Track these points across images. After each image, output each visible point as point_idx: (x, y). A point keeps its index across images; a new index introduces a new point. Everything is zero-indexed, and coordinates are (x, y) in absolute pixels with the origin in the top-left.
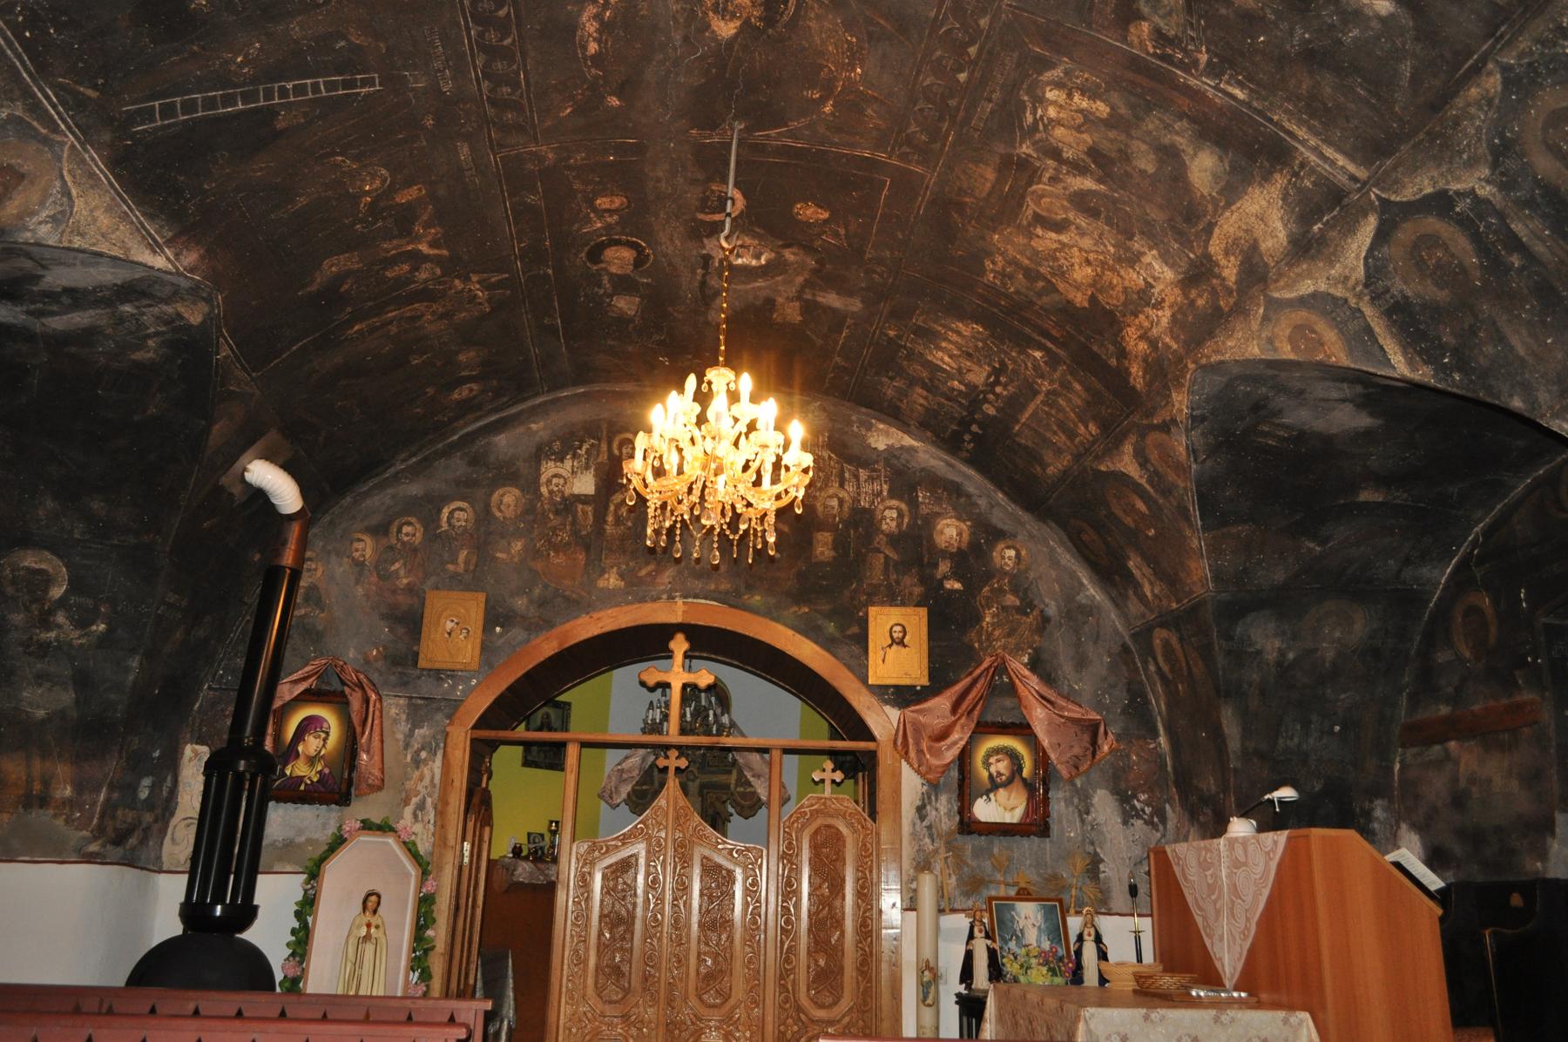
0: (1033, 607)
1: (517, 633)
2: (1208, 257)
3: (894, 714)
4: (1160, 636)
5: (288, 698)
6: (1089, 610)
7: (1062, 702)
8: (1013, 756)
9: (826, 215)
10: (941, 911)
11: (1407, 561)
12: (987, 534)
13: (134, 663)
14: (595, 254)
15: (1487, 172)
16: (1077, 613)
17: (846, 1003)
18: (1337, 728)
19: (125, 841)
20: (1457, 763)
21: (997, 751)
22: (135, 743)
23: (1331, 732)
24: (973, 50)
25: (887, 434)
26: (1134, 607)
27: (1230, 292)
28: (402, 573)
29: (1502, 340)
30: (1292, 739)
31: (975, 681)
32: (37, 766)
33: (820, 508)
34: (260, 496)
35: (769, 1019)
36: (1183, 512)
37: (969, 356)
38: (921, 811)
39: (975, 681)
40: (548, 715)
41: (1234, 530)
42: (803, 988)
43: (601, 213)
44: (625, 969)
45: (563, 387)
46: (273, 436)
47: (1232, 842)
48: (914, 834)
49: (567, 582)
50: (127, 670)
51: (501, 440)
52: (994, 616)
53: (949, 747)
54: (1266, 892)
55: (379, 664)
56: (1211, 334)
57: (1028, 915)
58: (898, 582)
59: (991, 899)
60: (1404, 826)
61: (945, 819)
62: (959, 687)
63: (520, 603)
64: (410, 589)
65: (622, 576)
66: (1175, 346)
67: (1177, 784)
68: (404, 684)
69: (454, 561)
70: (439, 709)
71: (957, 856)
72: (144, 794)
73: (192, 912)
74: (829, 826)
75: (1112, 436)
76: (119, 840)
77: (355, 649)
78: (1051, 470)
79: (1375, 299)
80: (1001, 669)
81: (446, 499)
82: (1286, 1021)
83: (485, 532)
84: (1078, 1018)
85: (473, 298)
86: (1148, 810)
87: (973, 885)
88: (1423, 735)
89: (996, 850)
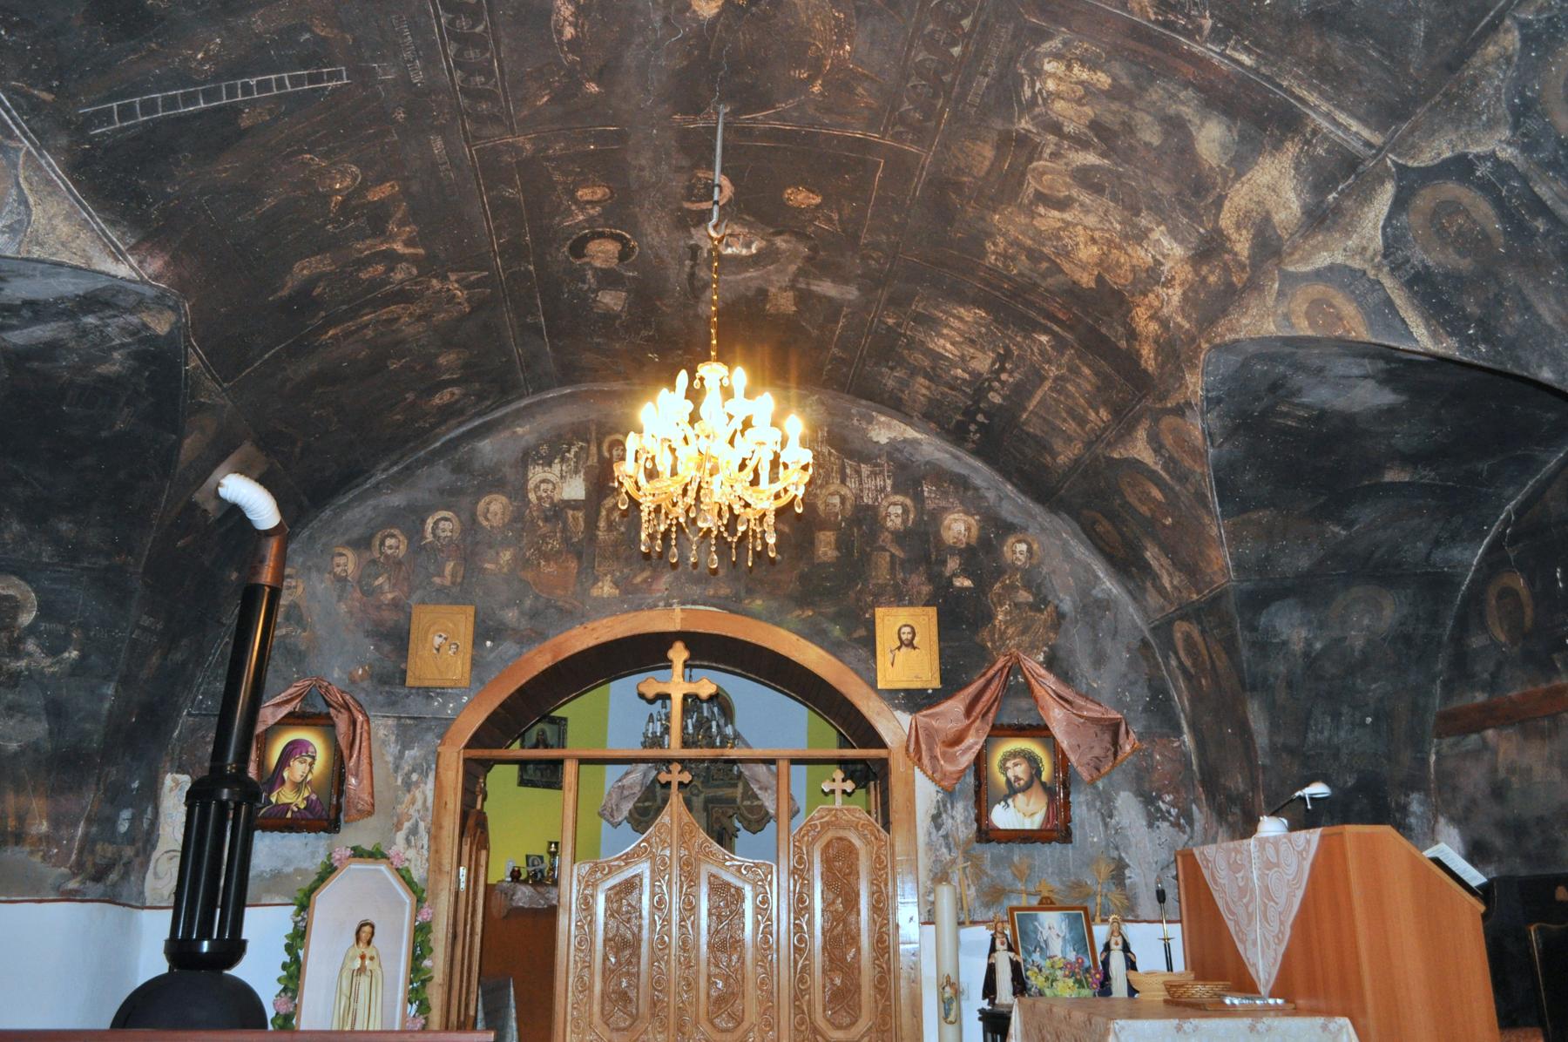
0: (1047, 603)
1: (509, 647)
3: (905, 719)
4: (1180, 629)
5: (271, 722)
6: (1105, 605)
7: (1080, 702)
8: (1031, 760)
9: (818, 200)
10: (961, 924)
11: (1437, 543)
12: (997, 528)
13: (110, 690)
14: (578, 248)
15: (1508, 133)
16: (1094, 608)
18: (1369, 720)
19: (105, 876)
21: (1014, 754)
22: (113, 773)
24: (966, 23)
25: (889, 427)
26: (1153, 600)
27: (1243, 267)
28: (386, 587)
29: (1528, 308)
30: (1322, 732)
33: (821, 507)
34: (235, 512)
37: (972, 341)
38: (936, 819)
39: (989, 682)
40: (543, 732)
41: (1254, 516)
42: (819, 1008)
43: (582, 205)
44: (632, 994)
45: (549, 388)
46: (247, 448)
47: (1263, 843)
48: (930, 845)
50: (102, 698)
52: (1006, 614)
53: (964, 752)
54: (1300, 894)
55: (366, 684)
57: (1052, 925)
58: (905, 582)
59: (1012, 909)
60: (1442, 820)
61: (962, 828)
62: (972, 690)
63: (511, 616)
64: (395, 605)
65: (616, 584)
66: (1187, 326)
67: (1203, 783)
68: (392, 703)
69: (441, 574)
70: (429, 729)
72: (123, 827)
73: (178, 950)
74: (841, 839)
76: (99, 876)
77: (341, 666)
78: (1061, 459)
80: (1016, 668)
81: (430, 509)
84: (1107, 1031)
85: (452, 298)
86: (1174, 811)
87: (994, 895)
88: (1458, 724)
89: (1016, 859)
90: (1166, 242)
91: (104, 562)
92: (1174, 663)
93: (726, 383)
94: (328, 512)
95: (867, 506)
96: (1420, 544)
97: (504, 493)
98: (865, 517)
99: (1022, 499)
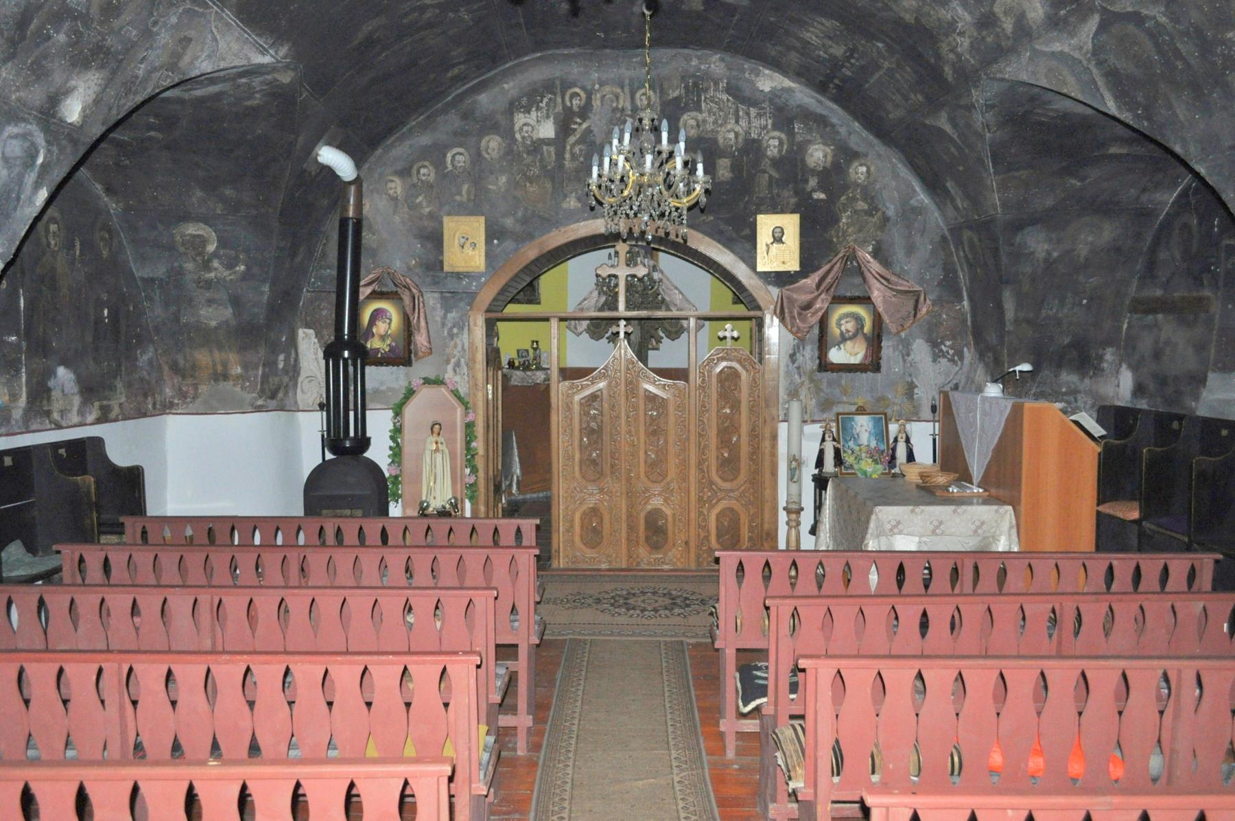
0: (877, 210)
1: (509, 244)
2: (994, 14)
3: (775, 291)
4: (967, 234)
6: (918, 211)
7: (893, 278)
8: (858, 319)
10: (805, 422)
11: (1144, 190)
12: (846, 155)
15: (1163, 9)
16: (910, 213)
17: (743, 476)
19: (275, 393)
20: (1160, 330)
22: (272, 335)
23: (1080, 304)
25: (771, 78)
26: (951, 212)
27: (1008, 38)
28: (424, 204)
29: (1170, 107)
31: (832, 267)
32: (217, 355)
33: (721, 141)
34: (328, 171)
35: (692, 489)
36: (980, 161)
37: (830, 38)
41: (1017, 174)
42: (714, 469)
47: (985, 399)
48: (788, 373)
49: (540, 205)
50: (262, 293)
51: (483, 98)
52: (848, 217)
53: (814, 314)
54: (999, 434)
56: (995, 61)
57: (863, 425)
58: (778, 195)
59: (838, 414)
60: (1124, 366)
61: (809, 362)
63: (509, 222)
64: (431, 216)
65: (579, 199)
66: (973, 62)
67: (974, 334)
68: (435, 283)
69: (460, 193)
70: (461, 299)
71: (816, 386)
72: (281, 365)
73: (333, 441)
75: (934, 104)
76: (273, 397)
78: (891, 116)
79: (1100, 63)
81: (448, 147)
82: (997, 511)
83: (479, 170)
84: (871, 513)
86: (951, 352)
87: (825, 405)
88: (1145, 307)
89: (843, 382)
90: (960, 10)
91: (254, 212)
92: (962, 254)
93: (656, 123)
94: (379, 151)
95: (754, 141)
96: (1132, 191)
97: (498, 134)
98: (752, 147)
99: (865, 133)
